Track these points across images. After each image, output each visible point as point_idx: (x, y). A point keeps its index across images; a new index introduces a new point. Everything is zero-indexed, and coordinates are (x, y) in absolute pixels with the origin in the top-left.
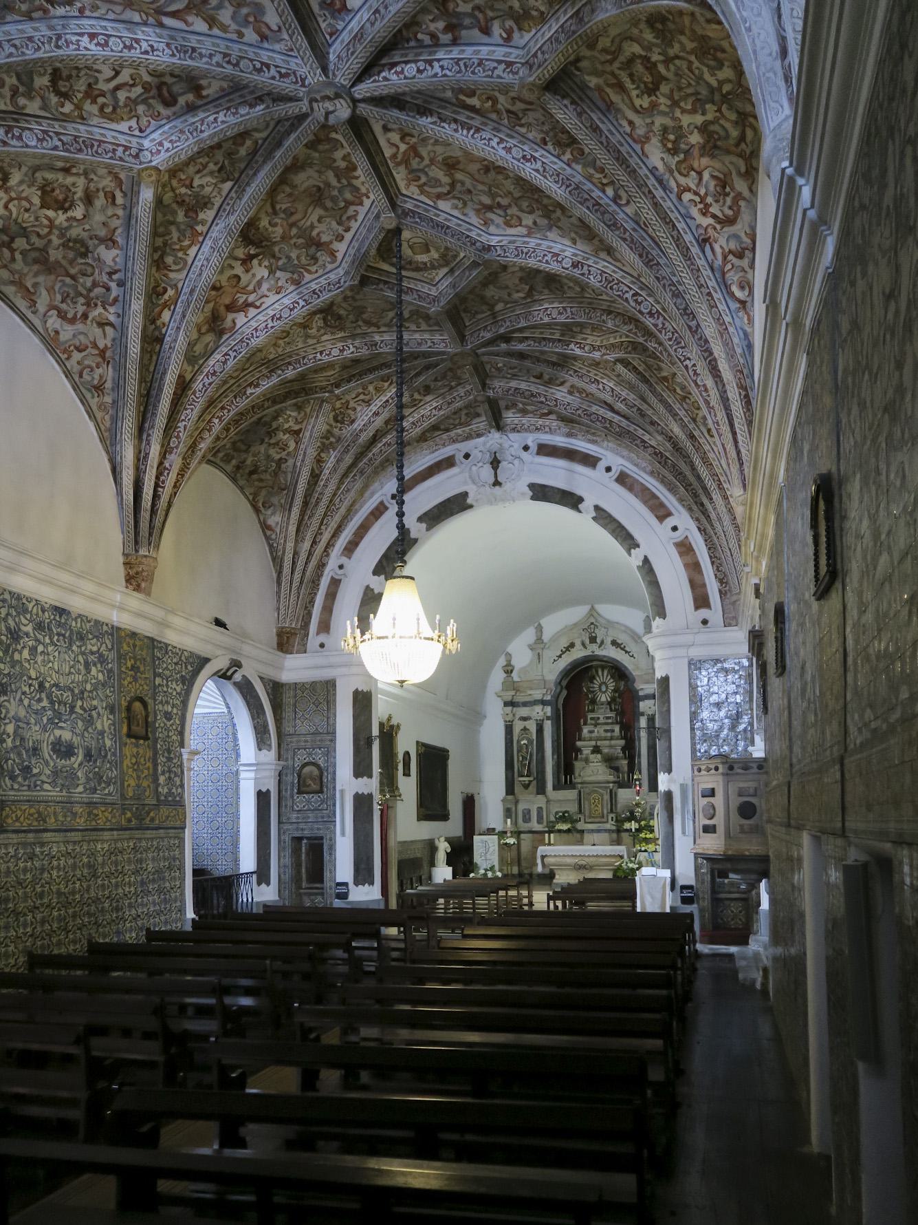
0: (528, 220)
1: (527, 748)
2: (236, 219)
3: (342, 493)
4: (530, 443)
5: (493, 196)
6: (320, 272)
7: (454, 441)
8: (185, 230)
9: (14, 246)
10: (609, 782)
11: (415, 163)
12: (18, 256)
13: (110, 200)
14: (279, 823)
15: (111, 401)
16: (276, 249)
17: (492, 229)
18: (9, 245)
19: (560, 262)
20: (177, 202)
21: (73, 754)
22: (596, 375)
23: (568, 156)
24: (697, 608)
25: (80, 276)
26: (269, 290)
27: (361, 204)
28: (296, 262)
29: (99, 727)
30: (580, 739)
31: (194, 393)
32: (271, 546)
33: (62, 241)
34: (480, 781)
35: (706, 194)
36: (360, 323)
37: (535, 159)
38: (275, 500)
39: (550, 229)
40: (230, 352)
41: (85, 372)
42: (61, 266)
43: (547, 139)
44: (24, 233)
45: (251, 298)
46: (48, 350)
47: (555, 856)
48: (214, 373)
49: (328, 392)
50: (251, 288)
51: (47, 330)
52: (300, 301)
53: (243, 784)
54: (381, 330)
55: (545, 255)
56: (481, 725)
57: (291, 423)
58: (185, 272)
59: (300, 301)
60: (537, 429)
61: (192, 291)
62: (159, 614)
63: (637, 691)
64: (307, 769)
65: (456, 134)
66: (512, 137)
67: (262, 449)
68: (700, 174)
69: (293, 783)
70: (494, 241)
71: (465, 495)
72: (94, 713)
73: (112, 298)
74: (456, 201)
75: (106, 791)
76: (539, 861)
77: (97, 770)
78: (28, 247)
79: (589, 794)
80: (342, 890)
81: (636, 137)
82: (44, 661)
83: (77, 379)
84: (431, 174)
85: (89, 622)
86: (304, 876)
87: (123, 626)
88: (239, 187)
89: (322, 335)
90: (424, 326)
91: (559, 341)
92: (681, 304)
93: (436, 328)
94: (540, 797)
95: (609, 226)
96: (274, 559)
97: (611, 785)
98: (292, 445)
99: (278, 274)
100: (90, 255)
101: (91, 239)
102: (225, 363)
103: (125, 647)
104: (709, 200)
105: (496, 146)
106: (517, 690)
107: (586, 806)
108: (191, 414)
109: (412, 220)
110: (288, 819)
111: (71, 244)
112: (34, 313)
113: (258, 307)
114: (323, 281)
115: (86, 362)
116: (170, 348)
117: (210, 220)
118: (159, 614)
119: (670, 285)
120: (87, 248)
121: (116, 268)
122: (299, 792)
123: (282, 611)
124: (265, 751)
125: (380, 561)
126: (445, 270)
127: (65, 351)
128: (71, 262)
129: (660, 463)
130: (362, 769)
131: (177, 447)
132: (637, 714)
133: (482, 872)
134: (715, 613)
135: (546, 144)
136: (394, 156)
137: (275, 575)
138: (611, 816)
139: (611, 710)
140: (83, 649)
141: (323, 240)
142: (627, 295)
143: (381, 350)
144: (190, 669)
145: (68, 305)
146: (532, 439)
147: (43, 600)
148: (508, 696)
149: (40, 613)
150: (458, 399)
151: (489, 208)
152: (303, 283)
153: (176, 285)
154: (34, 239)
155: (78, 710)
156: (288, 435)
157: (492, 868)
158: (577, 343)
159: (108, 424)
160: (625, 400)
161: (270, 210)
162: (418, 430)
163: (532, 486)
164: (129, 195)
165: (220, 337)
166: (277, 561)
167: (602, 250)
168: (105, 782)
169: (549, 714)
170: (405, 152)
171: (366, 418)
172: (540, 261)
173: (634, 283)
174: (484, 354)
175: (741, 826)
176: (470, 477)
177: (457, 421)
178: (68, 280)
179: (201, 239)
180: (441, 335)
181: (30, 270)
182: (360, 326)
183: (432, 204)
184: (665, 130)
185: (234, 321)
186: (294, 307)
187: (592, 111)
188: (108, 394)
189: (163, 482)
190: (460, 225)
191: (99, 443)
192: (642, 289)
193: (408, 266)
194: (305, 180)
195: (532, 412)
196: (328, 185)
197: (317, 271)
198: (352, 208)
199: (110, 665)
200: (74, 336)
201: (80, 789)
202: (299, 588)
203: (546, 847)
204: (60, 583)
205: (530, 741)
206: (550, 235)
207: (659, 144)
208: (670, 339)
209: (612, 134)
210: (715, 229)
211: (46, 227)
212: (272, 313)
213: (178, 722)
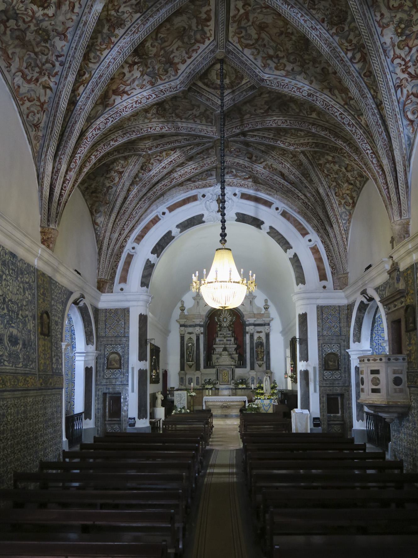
0: (289, 67)
1: (191, 348)
2: (138, 37)
3: (137, 209)
4: (237, 193)
5: (276, 49)
6: (167, 80)
7: (197, 188)
8: (105, 38)
9: (8, 24)
10: (232, 365)
11: (243, 23)
12: (8, 32)
13: (71, 8)
14: (96, 385)
15: (41, 135)
16: (149, 61)
17: (267, 70)
18: (4, 23)
19: (302, 93)
20: (107, 19)
21: (18, 343)
22: (282, 160)
23: (334, 31)
24: (321, 280)
25: (40, 54)
26: (137, 86)
27: (203, 43)
28: (156, 72)
29: (29, 328)
30: (215, 344)
31: (87, 139)
32: (96, 234)
33: (36, 28)
34: (167, 364)
35: (410, 61)
36: (173, 115)
37: (317, 29)
38: (102, 209)
39: (300, 74)
40: (110, 118)
41: (30, 115)
42: (31, 45)
43: (326, 19)
44: (16, 17)
45: (127, 88)
46: (13, 96)
47: (212, 401)
48: (99, 129)
49: (145, 152)
50: (128, 82)
51: (14, 84)
52: (153, 95)
53: (77, 363)
54: (182, 121)
55: (293, 88)
56: (168, 336)
57: (119, 167)
58: (98, 65)
59: (153, 95)
60: (241, 185)
61: (101, 77)
62: (55, 263)
63: (245, 322)
64: (113, 356)
65: (282, 6)
66: (307, 15)
67: (102, 179)
68: (411, 49)
69: (104, 363)
70: (266, 77)
71: (202, 216)
72: (27, 319)
73: (55, 71)
74: (254, 50)
75: (31, 367)
76: (204, 404)
77: (28, 353)
78: (16, 27)
79: (222, 371)
80: (132, 421)
81: (381, 24)
82: (5, 285)
83: (25, 118)
84: (249, 32)
85: (25, 264)
86: (107, 414)
87: (39, 269)
88: (144, 17)
89: (152, 119)
90: (204, 122)
91: (272, 139)
92: (375, 120)
93: (210, 124)
94: (198, 372)
95: (346, 73)
96: (97, 242)
97: (233, 366)
98: (117, 179)
99: (145, 77)
100: (49, 42)
101: (53, 31)
102: (106, 124)
103: (40, 282)
104: (410, 64)
105: (300, 18)
106: (187, 319)
107: (220, 376)
108: (83, 150)
109: (231, 56)
110: (101, 383)
111: (40, 32)
112: (9, 71)
113: (128, 95)
114: (167, 85)
115: (32, 109)
116: (81, 109)
117: (121, 35)
118: (55, 263)
119: (371, 109)
120: (49, 36)
121: (62, 53)
122: (108, 368)
123: (101, 270)
124: (90, 346)
125: (155, 247)
126: (230, 91)
127: (21, 99)
128: (38, 44)
129: (306, 207)
130: (142, 357)
131: (74, 168)
132: (244, 333)
133: (179, 410)
134: (329, 283)
135: (323, 22)
136: (235, 16)
137: (97, 250)
138: (232, 381)
139: (229, 330)
140: (23, 279)
141: (174, 61)
142: (336, 114)
143: (181, 132)
144: (65, 297)
145: (29, 71)
146: (238, 190)
147: (6, 247)
148: (183, 321)
149: (4, 255)
150: (207, 165)
151: (270, 57)
152: (156, 85)
153: (91, 72)
154: (20, 23)
155: (20, 316)
156: (116, 174)
157: (184, 408)
158: (282, 141)
159: (38, 149)
160: (294, 174)
161: (154, 37)
162: (183, 179)
163: (238, 214)
164: (83, 6)
165: (105, 109)
166: (100, 243)
167: (327, 88)
168: (31, 361)
169: (202, 331)
170: (241, 16)
171: (158, 170)
172: (290, 90)
173: (341, 108)
174: (231, 141)
175: (395, 389)
176: (206, 207)
177: (201, 177)
178: (33, 55)
179: (112, 46)
180: (212, 128)
181: (12, 43)
182: (173, 117)
183: (241, 49)
184: (401, 21)
185: (114, 101)
186: (149, 98)
187: (365, 4)
188: (41, 131)
189: (65, 187)
190: (251, 65)
191: (33, 160)
192: (344, 111)
193: (211, 86)
194: (179, 22)
195: (240, 177)
196: (190, 27)
197: (165, 79)
198: (198, 45)
199: (33, 291)
200: (28, 91)
201: (21, 365)
202: (110, 258)
203: (207, 397)
204: (15, 238)
205: (193, 345)
206: (298, 77)
207: (393, 30)
208: (359, 139)
209: (370, 20)
210: (407, 80)
211: (29, 16)
212: (136, 99)
213: (60, 327)
